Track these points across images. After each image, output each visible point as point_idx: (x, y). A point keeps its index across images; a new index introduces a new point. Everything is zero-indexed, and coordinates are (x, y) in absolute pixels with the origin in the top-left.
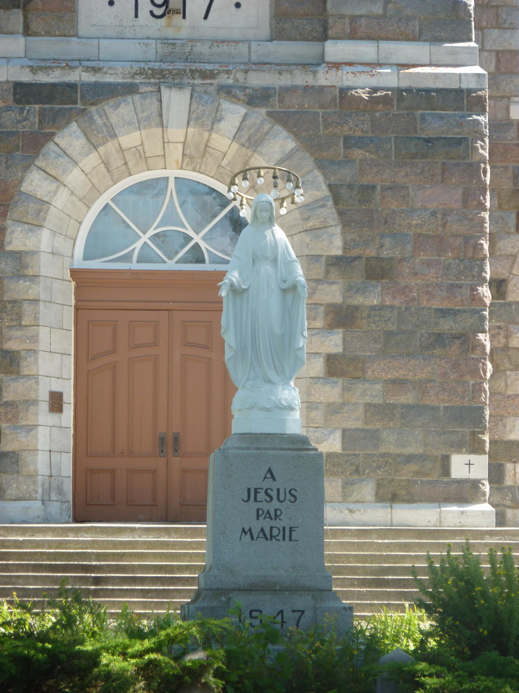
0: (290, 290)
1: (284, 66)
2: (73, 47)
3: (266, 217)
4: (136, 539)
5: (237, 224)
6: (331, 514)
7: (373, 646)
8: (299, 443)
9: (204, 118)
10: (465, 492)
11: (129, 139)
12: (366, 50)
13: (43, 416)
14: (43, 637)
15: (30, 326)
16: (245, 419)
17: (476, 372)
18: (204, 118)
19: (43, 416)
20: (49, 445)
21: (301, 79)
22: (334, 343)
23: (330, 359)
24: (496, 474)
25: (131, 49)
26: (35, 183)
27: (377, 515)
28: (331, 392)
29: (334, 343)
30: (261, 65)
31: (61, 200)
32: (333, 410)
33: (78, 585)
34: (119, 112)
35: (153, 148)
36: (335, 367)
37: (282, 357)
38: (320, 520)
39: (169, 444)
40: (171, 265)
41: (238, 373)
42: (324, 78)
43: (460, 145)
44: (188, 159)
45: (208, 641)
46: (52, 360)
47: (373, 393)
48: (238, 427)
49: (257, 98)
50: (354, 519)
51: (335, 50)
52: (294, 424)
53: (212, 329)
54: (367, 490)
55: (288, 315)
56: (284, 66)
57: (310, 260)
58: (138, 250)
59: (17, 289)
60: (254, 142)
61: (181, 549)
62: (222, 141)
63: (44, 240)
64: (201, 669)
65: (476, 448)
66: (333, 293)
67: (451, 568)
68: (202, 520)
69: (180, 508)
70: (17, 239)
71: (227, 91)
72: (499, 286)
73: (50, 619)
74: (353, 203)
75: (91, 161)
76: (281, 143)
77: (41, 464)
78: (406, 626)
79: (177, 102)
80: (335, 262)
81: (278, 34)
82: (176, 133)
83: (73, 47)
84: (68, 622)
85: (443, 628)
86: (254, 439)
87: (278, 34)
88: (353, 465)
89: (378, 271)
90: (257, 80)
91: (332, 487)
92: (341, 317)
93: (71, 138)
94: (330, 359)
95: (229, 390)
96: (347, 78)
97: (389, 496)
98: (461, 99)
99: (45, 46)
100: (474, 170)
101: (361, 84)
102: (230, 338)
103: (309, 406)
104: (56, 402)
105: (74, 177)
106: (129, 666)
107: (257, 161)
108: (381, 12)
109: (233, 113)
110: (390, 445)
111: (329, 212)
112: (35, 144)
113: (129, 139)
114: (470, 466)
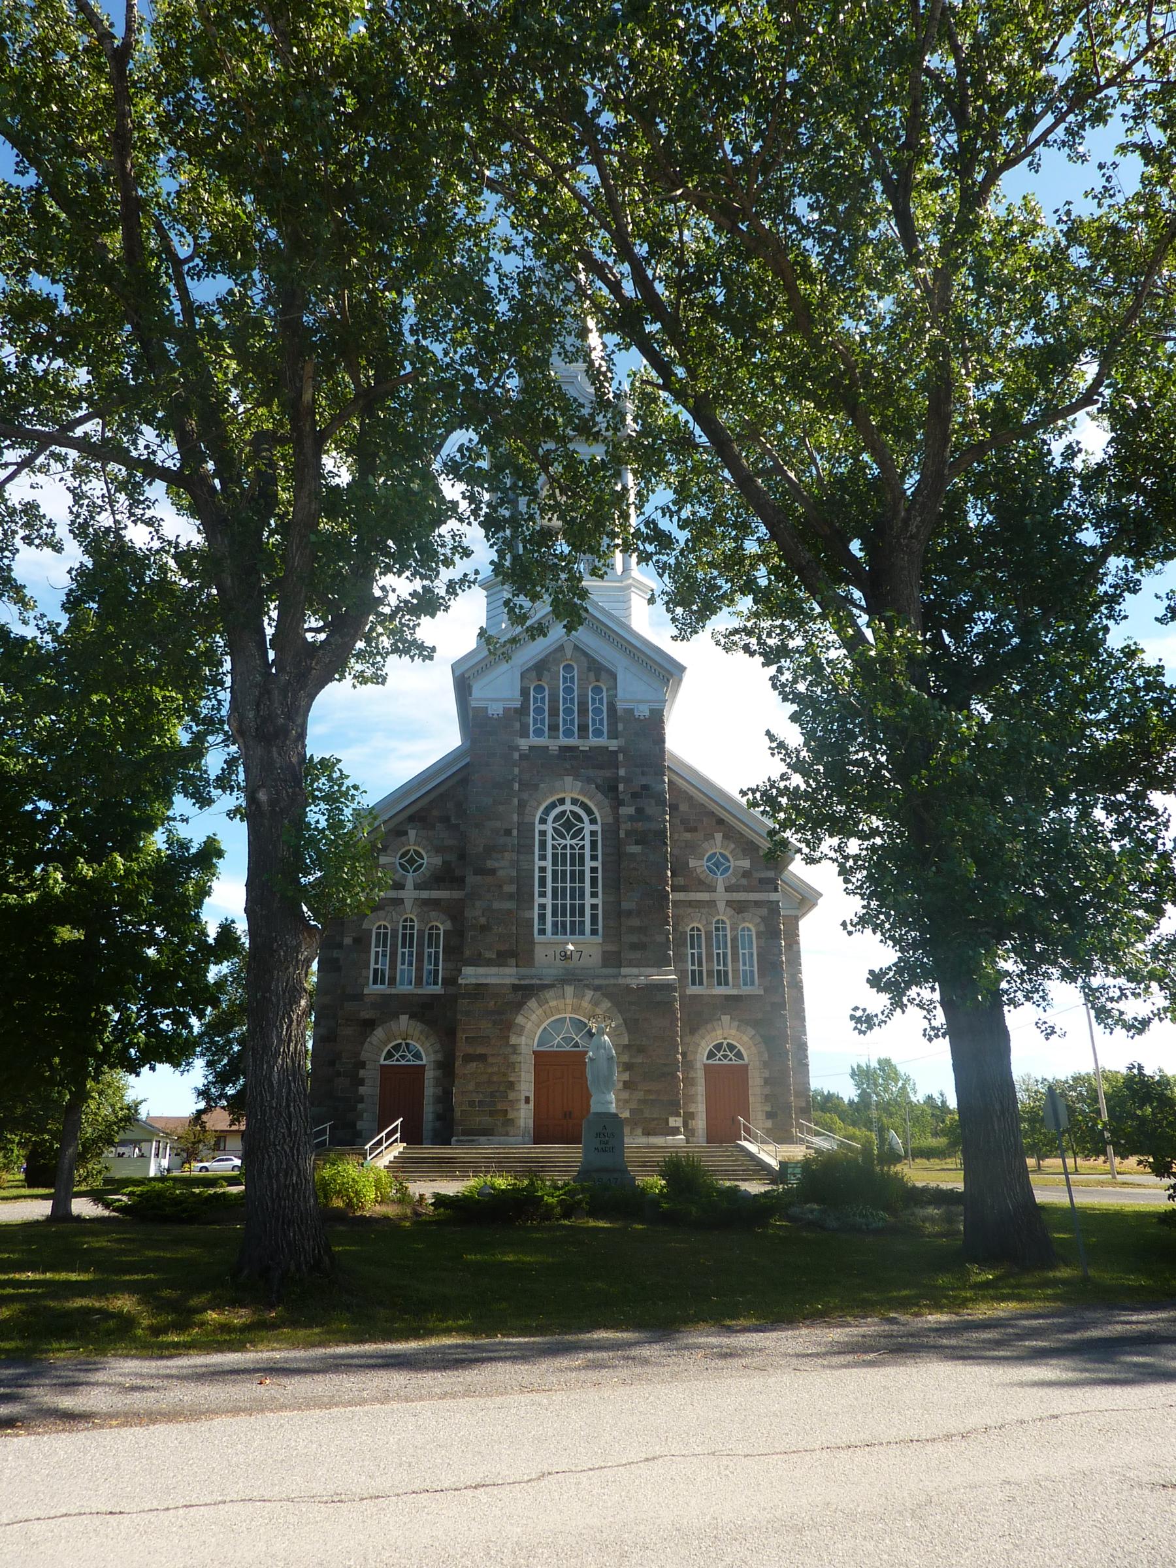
0: (610, 1058)
1: (606, 977)
2: (533, 971)
3: (601, 1032)
4: (556, 1150)
5: (590, 1034)
6: (626, 1140)
7: (643, 1191)
8: (616, 1115)
9: (579, 996)
10: (675, 1131)
11: (553, 1003)
12: (635, 971)
13: (523, 1105)
14: (523, 1189)
15: (825, 1354)
16: (594, 1108)
17: (678, 1086)
18: (579, 996)
19: (523, 1105)
20: (525, 1115)
21: (613, 981)
22: (626, 1076)
23: (625, 1082)
24: (685, 1124)
25: (553, 971)
26: (520, 1020)
27: (642, 1140)
28: (625, 1095)
29: (626, 1076)
30: (598, 977)
31: (529, 1025)
32: (626, 1101)
33: (533, 1169)
34: (549, 994)
35: (561, 1006)
36: (627, 1085)
37: (607, 1083)
38: (622, 1142)
39: (568, 1115)
40: (568, 1049)
41: (592, 1090)
42: (621, 981)
43: (669, 1004)
44: (574, 1011)
45: (583, 1190)
46: (526, 1085)
47: (640, 1095)
48: (592, 1110)
49: (597, 988)
50: (635, 1142)
51: (624, 971)
52: (613, 1108)
53: (583, 1073)
54: (639, 1131)
55: (610, 1069)
56: (606, 977)
57: (616, 1046)
58: (556, 1043)
59: (514, 1058)
60: (596, 1004)
61: (571, 1154)
62: (585, 1004)
63: (523, 1040)
64: (580, 1202)
65: (678, 1115)
66: (625, 1058)
67: (671, 1161)
68: (577, 1141)
69: (574, 1139)
70: (514, 1040)
71: (587, 986)
72: (684, 1054)
73: (526, 1182)
74: (631, 1025)
75: (540, 1012)
76: (606, 1004)
77: (522, 1123)
78: (657, 1183)
79: (569, 990)
80: (626, 1047)
81: (604, 966)
82: (569, 1001)
83: (533, 971)
84: (532, 1184)
85: (668, 1185)
86: (598, 1114)
87: (604, 966)
88: (634, 1122)
89: (641, 1050)
90: (597, 982)
91: (626, 1130)
92: (628, 1067)
93: (532, 1003)
94: (625, 1082)
95: (589, 1096)
96: (628, 981)
97: (647, 1133)
98: (667, 987)
99: (524, 971)
100: (674, 1013)
101: (634, 983)
102: (589, 1076)
103: (618, 1100)
104: (527, 1100)
105: (534, 1017)
106: (554, 1200)
107: (598, 1011)
108: (182, 256)
109: (589, 994)
110: (647, 1115)
111: (623, 1029)
112: (519, 1006)
113: (553, 1003)
114: (674, 1122)
